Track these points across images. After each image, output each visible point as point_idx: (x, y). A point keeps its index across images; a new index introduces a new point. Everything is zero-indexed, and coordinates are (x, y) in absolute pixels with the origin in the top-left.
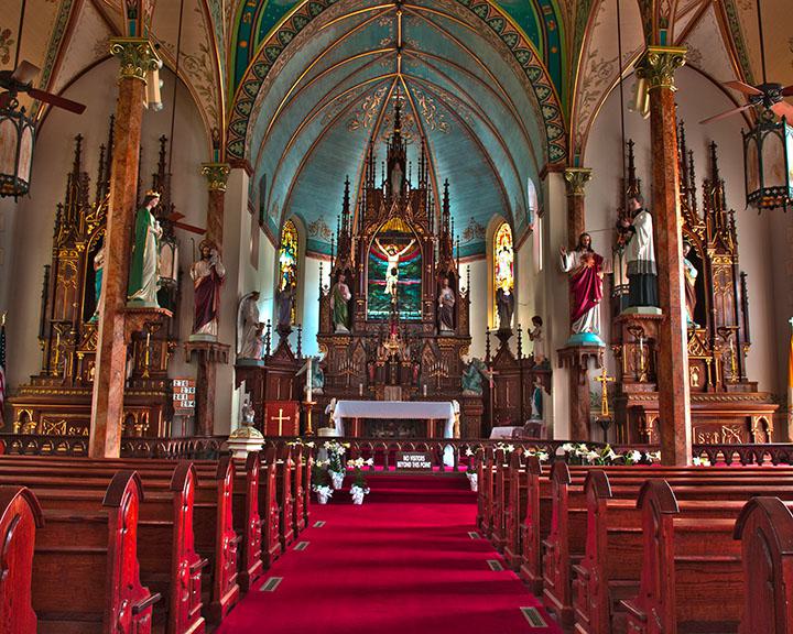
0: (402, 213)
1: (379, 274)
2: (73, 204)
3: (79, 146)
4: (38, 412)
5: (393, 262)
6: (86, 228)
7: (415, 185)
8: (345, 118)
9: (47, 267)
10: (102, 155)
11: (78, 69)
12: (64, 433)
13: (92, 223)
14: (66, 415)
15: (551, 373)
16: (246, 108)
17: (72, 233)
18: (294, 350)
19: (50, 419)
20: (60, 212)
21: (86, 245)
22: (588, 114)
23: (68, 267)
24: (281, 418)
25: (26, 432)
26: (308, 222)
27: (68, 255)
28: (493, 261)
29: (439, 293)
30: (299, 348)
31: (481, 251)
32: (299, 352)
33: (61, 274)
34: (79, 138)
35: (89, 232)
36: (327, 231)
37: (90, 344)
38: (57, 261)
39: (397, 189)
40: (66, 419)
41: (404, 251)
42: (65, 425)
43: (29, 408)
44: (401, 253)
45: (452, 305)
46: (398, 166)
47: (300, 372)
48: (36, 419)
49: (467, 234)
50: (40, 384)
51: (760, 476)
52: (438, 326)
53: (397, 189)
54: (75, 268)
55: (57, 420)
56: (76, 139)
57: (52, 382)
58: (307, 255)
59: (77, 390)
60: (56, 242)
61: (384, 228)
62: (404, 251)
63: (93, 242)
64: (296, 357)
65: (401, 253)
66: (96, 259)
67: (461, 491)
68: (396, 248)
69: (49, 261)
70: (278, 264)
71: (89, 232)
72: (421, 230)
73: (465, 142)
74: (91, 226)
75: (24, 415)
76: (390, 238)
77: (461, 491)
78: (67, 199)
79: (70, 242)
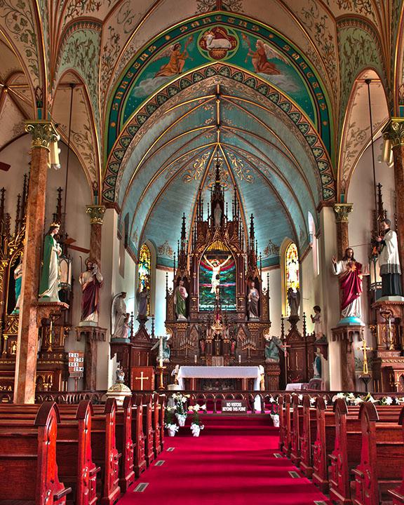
0: (222, 237)
5: (216, 271)
6: (9, 251)
8: (183, 173)
10: (19, 202)
13: (13, 247)
18: (149, 332)
26: (157, 245)
29: (248, 292)
30: (153, 331)
31: (277, 263)
32: (153, 334)
34: (3, 190)
35: (11, 254)
36: (170, 251)
39: (218, 221)
41: (224, 264)
44: (221, 265)
45: (257, 300)
46: (218, 205)
47: (154, 347)
49: (266, 251)
52: (248, 314)
53: (218, 221)
58: (157, 268)
61: (210, 249)
62: (224, 264)
64: (151, 337)
65: (221, 265)
66: (16, 272)
68: (218, 262)
70: (137, 274)
71: (11, 254)
72: (235, 249)
73: (264, 188)
74: (12, 250)
76: (213, 255)
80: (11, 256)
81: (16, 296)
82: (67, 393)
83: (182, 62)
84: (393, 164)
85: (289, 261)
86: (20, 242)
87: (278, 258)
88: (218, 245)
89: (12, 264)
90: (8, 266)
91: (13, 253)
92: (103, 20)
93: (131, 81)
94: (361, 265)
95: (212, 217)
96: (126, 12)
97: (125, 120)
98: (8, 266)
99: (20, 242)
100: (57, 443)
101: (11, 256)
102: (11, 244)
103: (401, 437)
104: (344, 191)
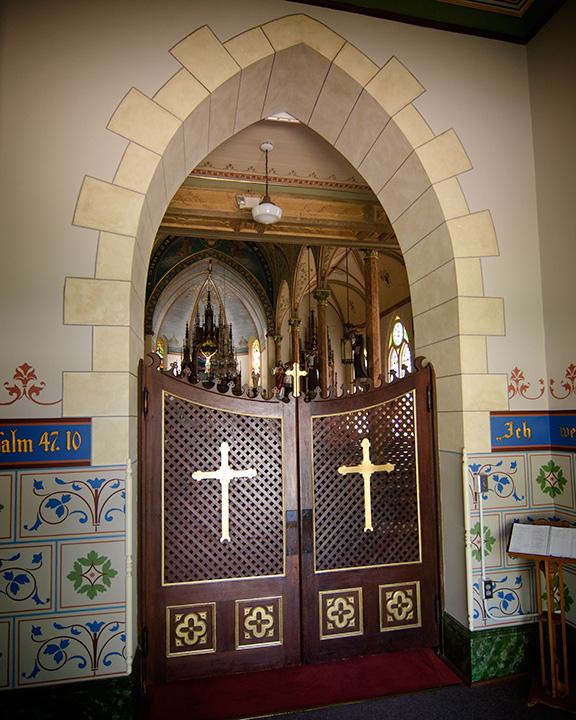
0: (212, 339)
1: (203, 364)
5: (208, 358)
7: (217, 324)
8: (186, 294)
16: (151, 310)
22: (283, 316)
24: (367, 469)
28: (251, 356)
31: (246, 351)
36: (177, 341)
39: (209, 327)
47: (377, 500)
49: (240, 343)
53: (209, 327)
61: (204, 345)
67: (394, 246)
73: (239, 305)
76: (206, 349)
77: (394, 246)
83: (190, 248)
85: (254, 350)
87: (247, 349)
88: (208, 343)
93: (159, 257)
95: (206, 325)
97: (157, 282)
103: (24, 441)
104: (279, 329)
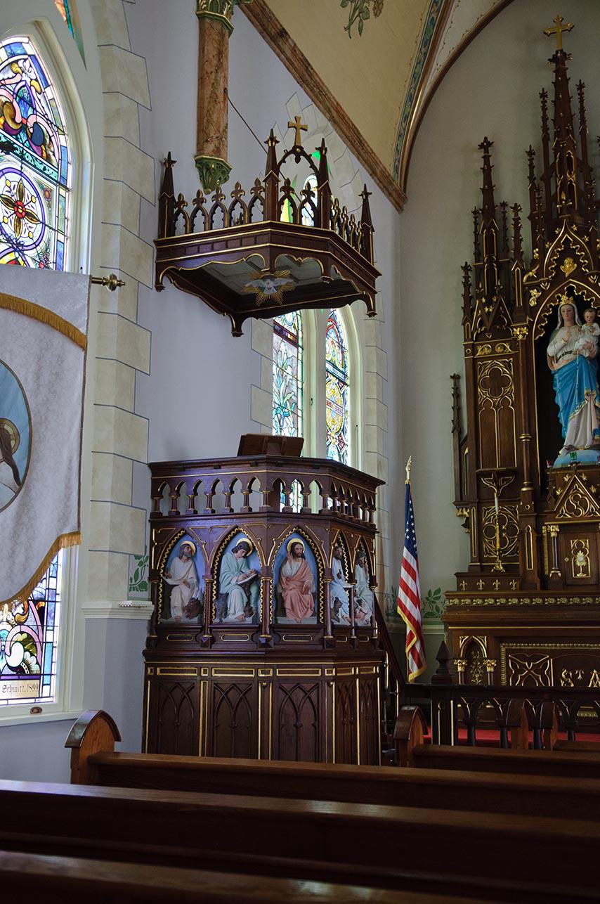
2: (490, 261)
3: (486, 159)
4: (498, 639)
6: (527, 296)
9: (456, 378)
10: (531, 167)
11: (470, 25)
12: (551, 683)
13: (537, 286)
14: (551, 646)
15: (150, 579)
17: (498, 312)
19: (520, 655)
20: (466, 278)
21: (530, 328)
23: (495, 373)
25: (477, 680)
27: (494, 351)
33: (485, 387)
34: (486, 146)
35: (533, 303)
37: (570, 508)
38: (473, 365)
40: (552, 653)
42: (550, 664)
43: (481, 633)
48: (494, 655)
50: (476, 588)
51: (288, 672)
54: (507, 374)
55: (534, 655)
56: (481, 146)
57: (497, 583)
59: (531, 597)
60: (467, 331)
63: (540, 320)
66: (551, 350)
69: (458, 365)
71: (533, 303)
74: (534, 292)
75: (472, 646)
78: (478, 255)
79: (498, 328)
80: (533, 311)
81: (561, 415)
82: (44, 675)
84: (407, 651)
86: (557, 268)
89: (537, 332)
90: (529, 336)
91: (539, 300)
92: (71, 749)
94: (372, 483)
96: (302, 123)
98: (529, 336)
99: (557, 268)
100: (272, 759)
101: (533, 311)
102: (529, 279)
